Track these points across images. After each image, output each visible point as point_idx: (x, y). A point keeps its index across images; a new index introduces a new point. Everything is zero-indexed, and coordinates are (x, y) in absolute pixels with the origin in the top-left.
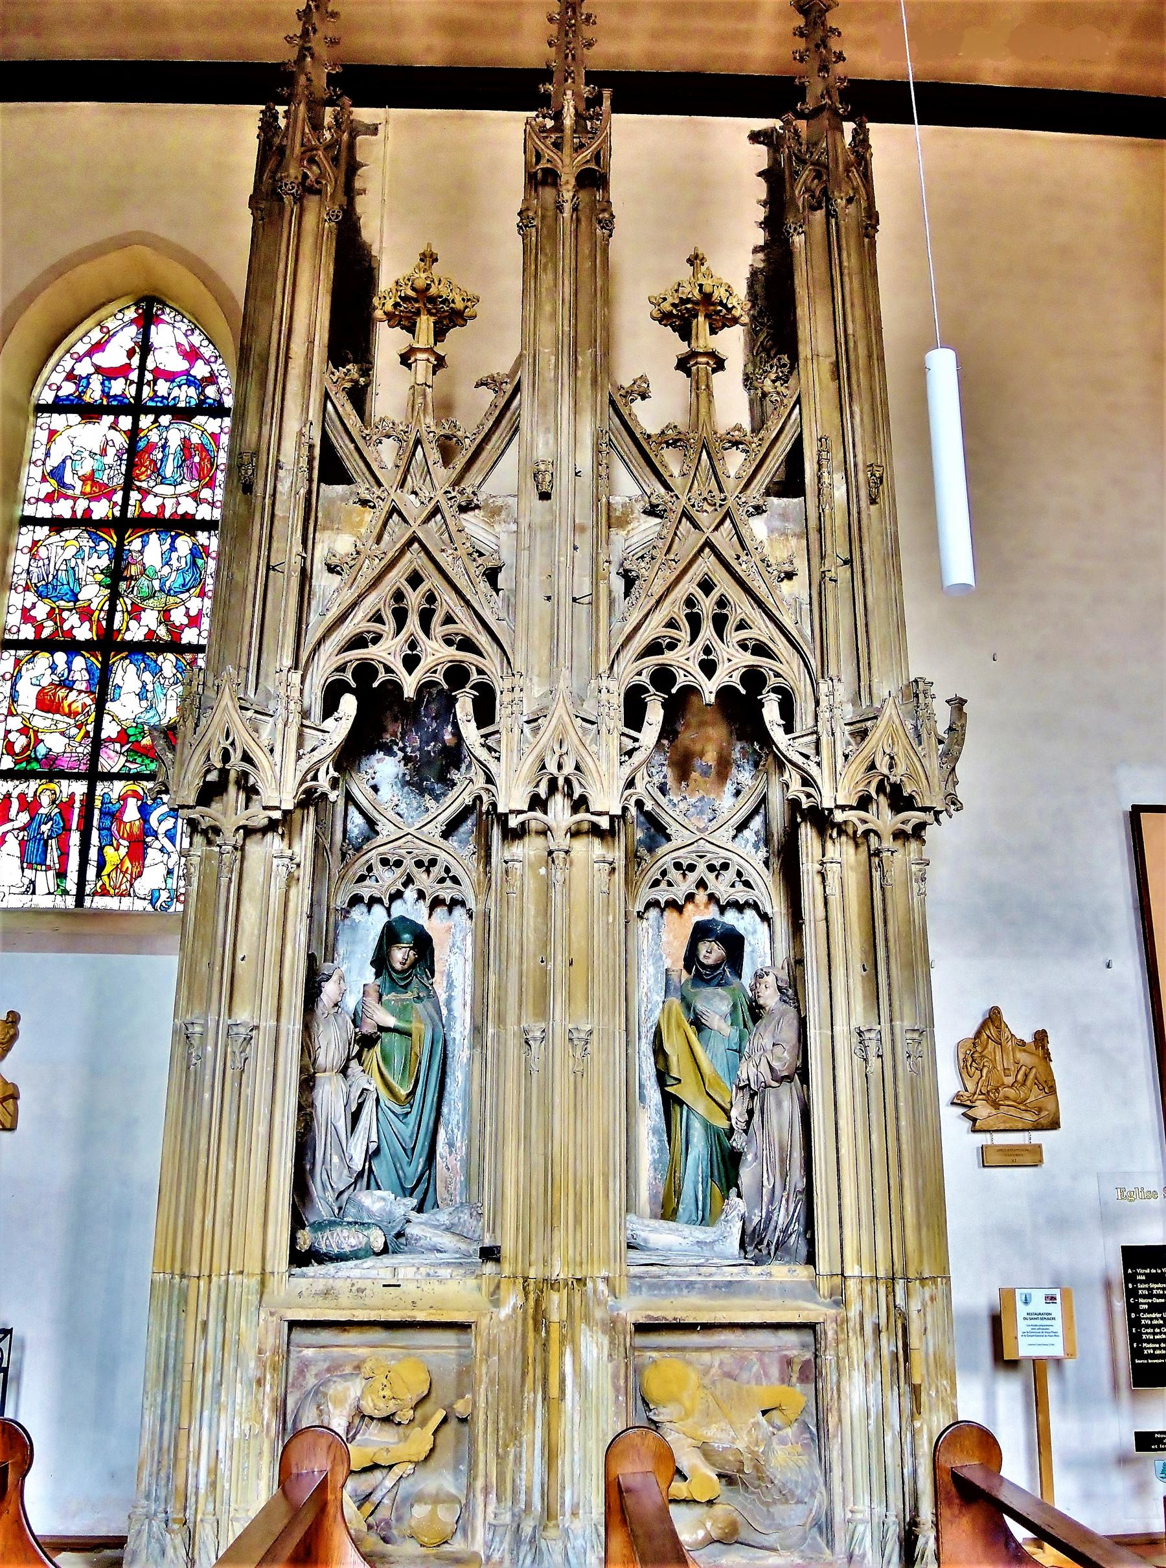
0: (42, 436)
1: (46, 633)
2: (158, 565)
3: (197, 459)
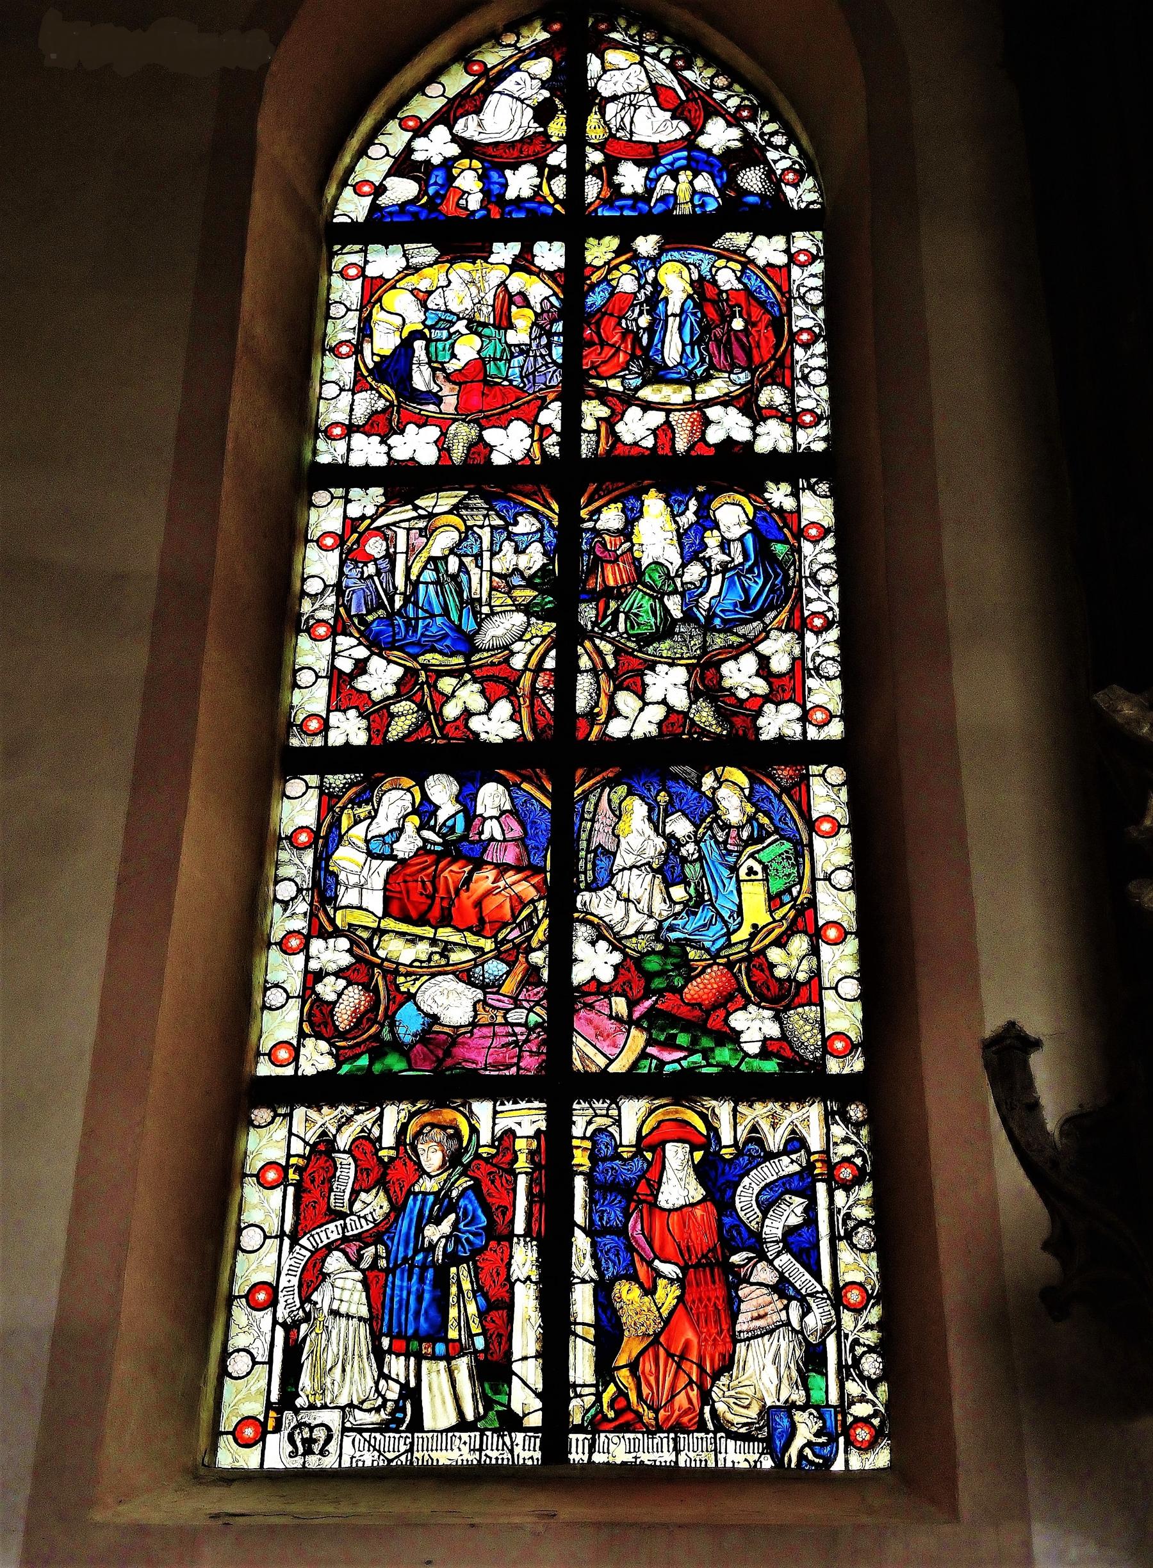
0: (348, 292)
1: (398, 729)
2: (673, 557)
3: (738, 324)
